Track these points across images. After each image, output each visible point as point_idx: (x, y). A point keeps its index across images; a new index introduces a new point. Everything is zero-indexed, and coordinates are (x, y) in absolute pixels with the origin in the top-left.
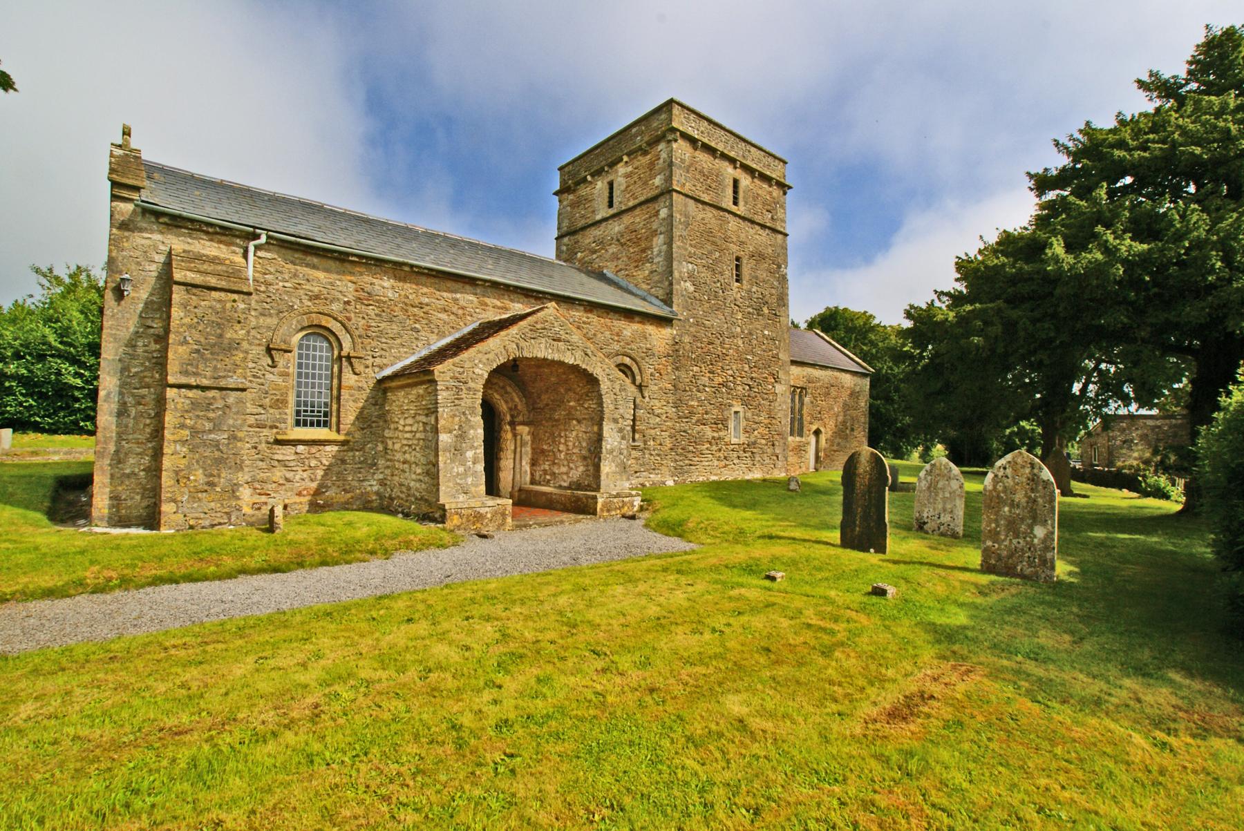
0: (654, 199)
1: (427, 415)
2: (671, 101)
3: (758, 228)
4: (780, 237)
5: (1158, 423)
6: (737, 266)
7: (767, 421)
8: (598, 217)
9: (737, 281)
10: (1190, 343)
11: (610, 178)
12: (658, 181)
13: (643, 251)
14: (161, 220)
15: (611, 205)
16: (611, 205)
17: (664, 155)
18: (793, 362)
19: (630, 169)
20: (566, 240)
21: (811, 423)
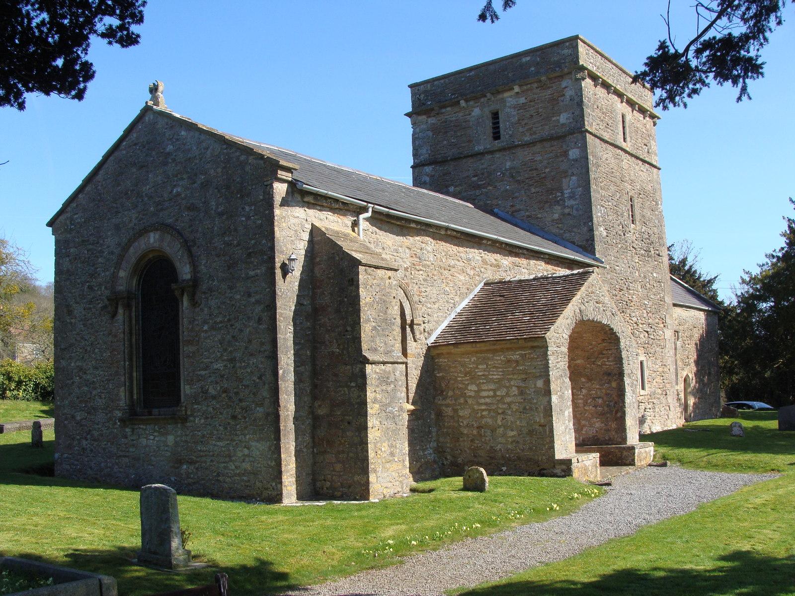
0: (561, 138)
1: (524, 380)
2: (576, 38)
3: (640, 163)
4: (655, 170)
5: (444, 402)
6: (632, 205)
7: (660, 370)
8: (479, 148)
9: (633, 223)
10: (68, 82)
11: (494, 107)
12: (563, 118)
13: (550, 191)
14: (306, 199)
15: (497, 136)
16: (497, 136)
17: (569, 93)
18: (675, 305)
19: (522, 100)
20: (428, 169)
21: (683, 369)
